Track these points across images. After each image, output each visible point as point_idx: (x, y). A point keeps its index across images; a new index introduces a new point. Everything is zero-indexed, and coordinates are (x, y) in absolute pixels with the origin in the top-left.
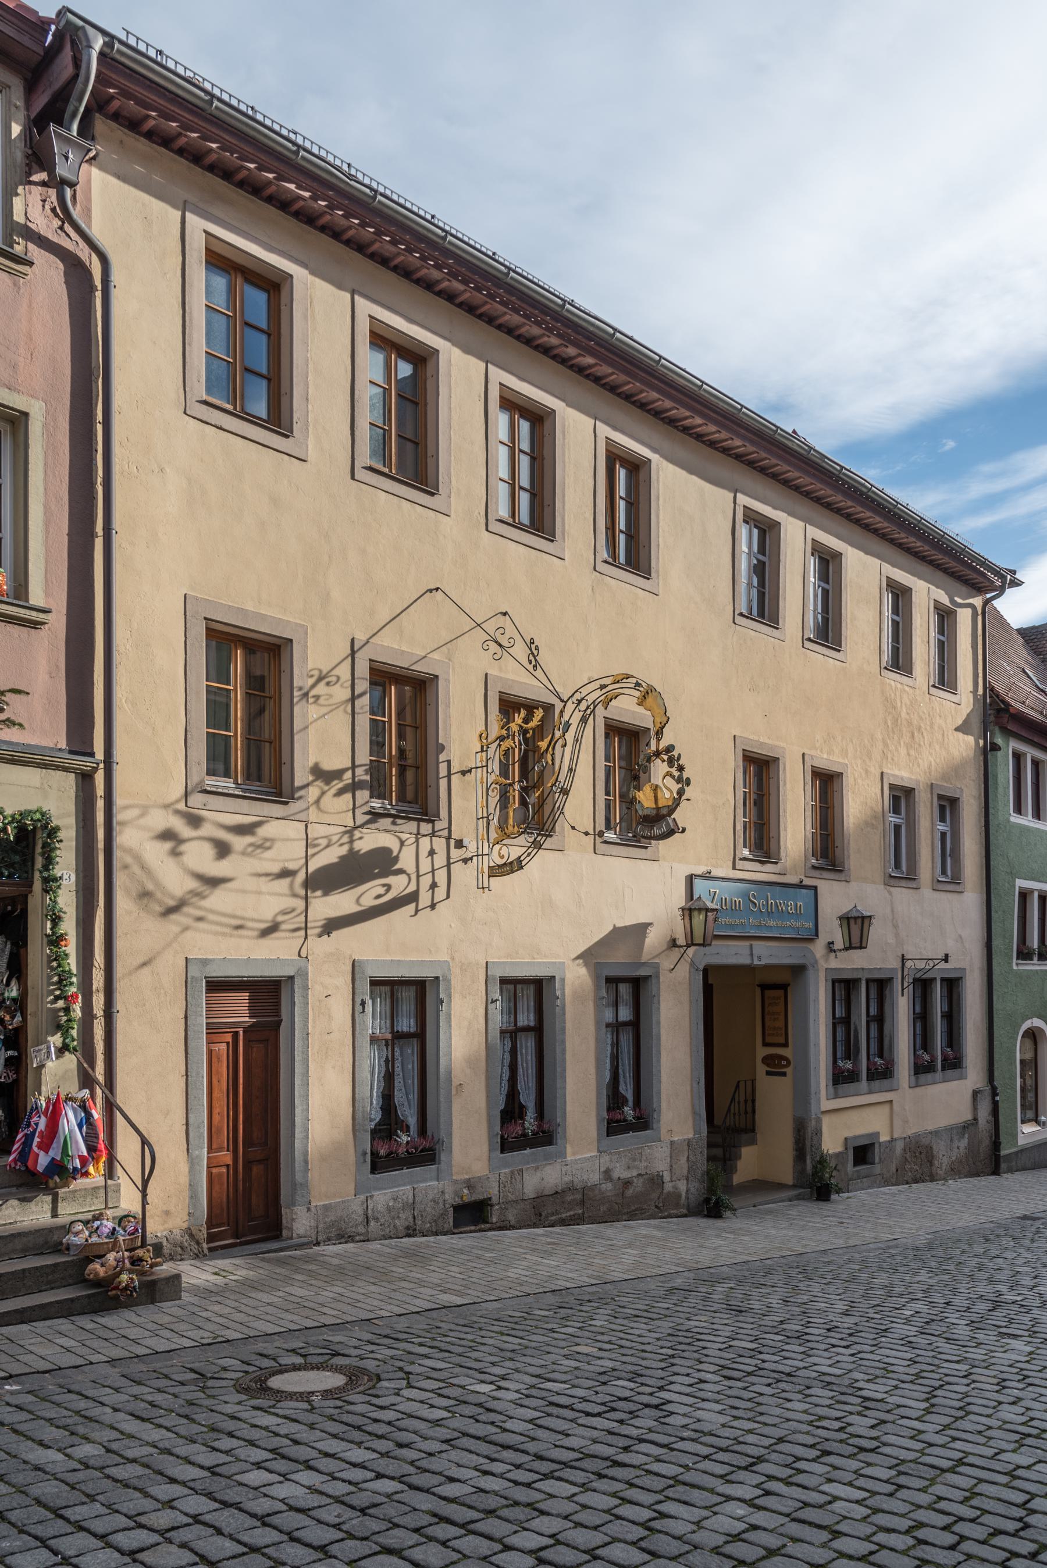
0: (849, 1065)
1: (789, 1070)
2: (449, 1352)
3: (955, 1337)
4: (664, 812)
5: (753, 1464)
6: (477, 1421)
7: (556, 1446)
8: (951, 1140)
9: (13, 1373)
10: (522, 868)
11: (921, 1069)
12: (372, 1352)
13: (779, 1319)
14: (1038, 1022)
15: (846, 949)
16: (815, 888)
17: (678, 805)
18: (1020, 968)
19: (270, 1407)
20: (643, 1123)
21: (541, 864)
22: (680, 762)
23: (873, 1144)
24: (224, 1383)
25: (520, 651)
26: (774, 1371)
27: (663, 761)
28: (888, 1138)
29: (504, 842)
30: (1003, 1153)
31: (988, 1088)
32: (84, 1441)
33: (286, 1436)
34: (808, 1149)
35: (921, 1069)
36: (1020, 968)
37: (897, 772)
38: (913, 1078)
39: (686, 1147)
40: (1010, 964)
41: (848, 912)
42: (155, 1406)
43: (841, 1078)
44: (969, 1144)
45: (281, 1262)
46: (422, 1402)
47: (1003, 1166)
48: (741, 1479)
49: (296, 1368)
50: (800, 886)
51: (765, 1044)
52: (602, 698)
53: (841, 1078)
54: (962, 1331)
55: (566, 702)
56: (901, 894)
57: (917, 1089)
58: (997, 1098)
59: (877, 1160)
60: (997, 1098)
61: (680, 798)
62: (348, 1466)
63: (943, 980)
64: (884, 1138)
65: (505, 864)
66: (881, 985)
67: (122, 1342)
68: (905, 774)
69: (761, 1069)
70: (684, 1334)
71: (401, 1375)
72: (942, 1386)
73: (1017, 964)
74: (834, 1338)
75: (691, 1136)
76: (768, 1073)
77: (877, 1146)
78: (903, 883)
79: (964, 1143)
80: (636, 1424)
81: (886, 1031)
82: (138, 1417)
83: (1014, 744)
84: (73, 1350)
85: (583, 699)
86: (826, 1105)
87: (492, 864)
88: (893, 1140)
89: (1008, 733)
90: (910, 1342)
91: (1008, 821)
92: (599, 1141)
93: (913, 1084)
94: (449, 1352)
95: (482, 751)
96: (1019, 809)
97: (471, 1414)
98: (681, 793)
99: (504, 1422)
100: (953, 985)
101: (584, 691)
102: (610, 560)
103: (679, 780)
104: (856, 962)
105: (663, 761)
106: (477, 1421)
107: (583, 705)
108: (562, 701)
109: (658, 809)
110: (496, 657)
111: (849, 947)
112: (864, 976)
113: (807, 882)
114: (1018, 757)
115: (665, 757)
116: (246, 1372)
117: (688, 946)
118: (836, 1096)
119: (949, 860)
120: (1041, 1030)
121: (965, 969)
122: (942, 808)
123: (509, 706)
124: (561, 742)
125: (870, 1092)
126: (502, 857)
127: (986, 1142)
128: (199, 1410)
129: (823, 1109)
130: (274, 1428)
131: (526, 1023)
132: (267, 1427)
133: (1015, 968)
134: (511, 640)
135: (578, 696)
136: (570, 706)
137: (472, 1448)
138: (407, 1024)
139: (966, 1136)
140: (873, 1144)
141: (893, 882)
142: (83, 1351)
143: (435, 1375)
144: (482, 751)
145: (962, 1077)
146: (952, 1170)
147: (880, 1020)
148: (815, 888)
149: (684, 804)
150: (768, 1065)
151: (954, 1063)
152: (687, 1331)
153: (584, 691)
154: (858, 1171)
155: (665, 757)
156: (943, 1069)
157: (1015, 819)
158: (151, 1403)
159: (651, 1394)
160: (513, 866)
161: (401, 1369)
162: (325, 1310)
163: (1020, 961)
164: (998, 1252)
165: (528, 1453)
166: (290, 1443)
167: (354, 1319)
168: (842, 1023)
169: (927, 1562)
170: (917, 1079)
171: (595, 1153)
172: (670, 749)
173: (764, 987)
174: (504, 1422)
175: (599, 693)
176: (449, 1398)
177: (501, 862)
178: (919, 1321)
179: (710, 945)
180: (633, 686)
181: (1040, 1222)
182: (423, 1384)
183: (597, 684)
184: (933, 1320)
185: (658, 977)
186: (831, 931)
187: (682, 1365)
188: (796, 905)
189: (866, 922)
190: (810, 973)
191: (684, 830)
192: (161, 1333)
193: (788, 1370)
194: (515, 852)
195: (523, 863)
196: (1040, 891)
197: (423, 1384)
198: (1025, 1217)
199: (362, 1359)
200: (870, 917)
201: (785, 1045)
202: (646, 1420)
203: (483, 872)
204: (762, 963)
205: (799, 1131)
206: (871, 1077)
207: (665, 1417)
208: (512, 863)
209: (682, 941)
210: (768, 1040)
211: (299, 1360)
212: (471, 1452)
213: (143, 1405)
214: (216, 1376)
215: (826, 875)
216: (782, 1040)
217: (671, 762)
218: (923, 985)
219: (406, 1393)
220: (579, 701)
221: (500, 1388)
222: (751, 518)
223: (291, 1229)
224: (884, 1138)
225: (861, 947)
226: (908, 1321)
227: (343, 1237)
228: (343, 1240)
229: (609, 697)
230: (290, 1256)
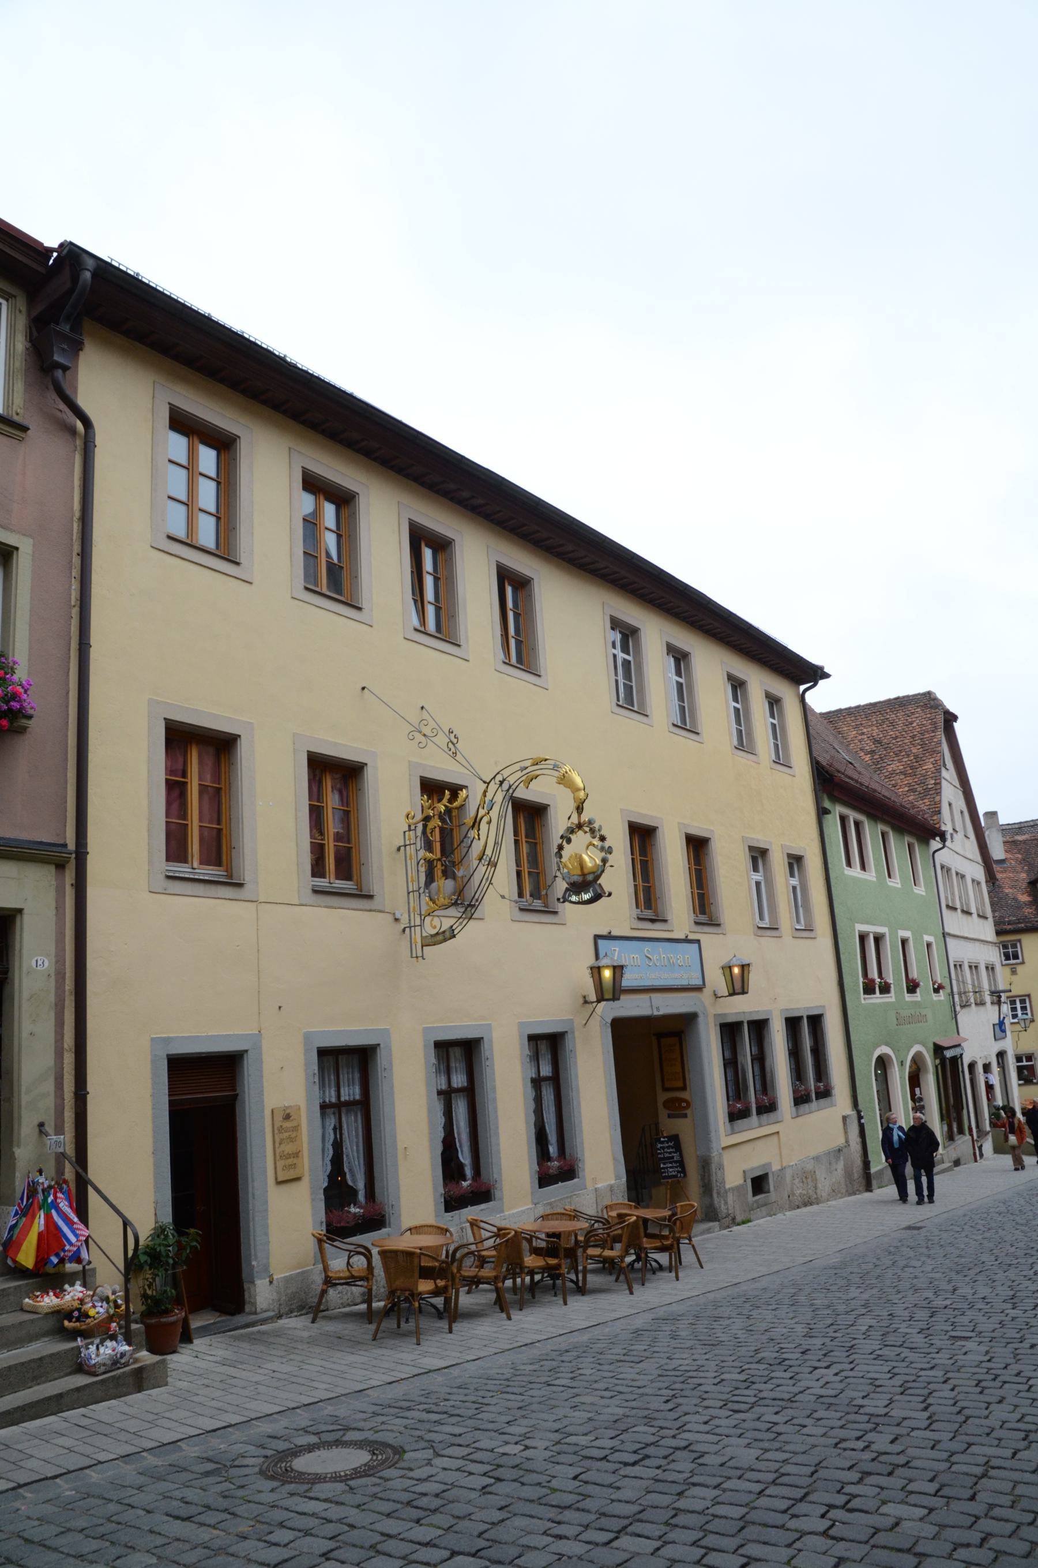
0: (289, 1148)
1: (688, 1112)
2: (459, 1415)
3: (914, 1345)
4: (590, 878)
5: (806, 1494)
6: (523, 1484)
7: (613, 1501)
8: (830, 1164)
9: (22, 1482)
10: (454, 936)
11: (800, 1099)
12: (383, 1423)
13: (753, 1348)
14: (885, 1050)
15: (730, 995)
16: (698, 941)
17: (603, 871)
18: (868, 1001)
19: (307, 1491)
20: (569, 1173)
21: (471, 933)
22: (602, 833)
23: (766, 1175)
24: (246, 1471)
25: (442, 740)
26: (774, 1399)
27: (586, 832)
28: (779, 1167)
29: (435, 913)
30: (873, 1170)
31: (854, 1113)
32: (130, 1551)
33: (340, 1521)
34: (714, 1185)
35: (800, 1099)
36: (868, 1001)
37: (753, 836)
38: (794, 1109)
39: (609, 1193)
40: (859, 998)
41: (730, 961)
42: (187, 1503)
43: (736, 1115)
44: (844, 1166)
45: (251, 1339)
46: (458, 1470)
47: (874, 1183)
48: (803, 1512)
49: (311, 1448)
50: (687, 940)
51: (665, 1089)
52: (524, 778)
53: (736, 1115)
54: (919, 1340)
55: (489, 783)
56: (767, 942)
57: (799, 1119)
58: (863, 1121)
59: (772, 1188)
60: (863, 1121)
61: (604, 865)
62: (418, 1547)
63: (750, 1023)
64: (776, 1167)
65: (437, 934)
66: (759, 1027)
67: (123, 1436)
68: (760, 837)
69: (663, 1113)
70: (673, 1373)
71: (424, 1444)
72: (930, 1393)
73: (864, 999)
74: (812, 1358)
75: (613, 1182)
76: (669, 1116)
77: (770, 1176)
78: (769, 933)
79: (840, 1166)
80: (678, 1469)
81: (768, 1069)
82: (177, 1518)
83: (838, 809)
84: (75, 1449)
85: (504, 780)
86: (726, 1141)
87: (424, 934)
88: (783, 1169)
89: (834, 799)
90: (879, 1356)
91: (843, 873)
92: (532, 1193)
93: (794, 1115)
94: (459, 1415)
95: (410, 830)
96: (849, 864)
97: (514, 1477)
98: (604, 861)
99: (549, 1482)
100: (816, 1021)
101: (506, 773)
102: (507, 661)
103: (602, 849)
104: (741, 1008)
105: (586, 832)
106: (523, 1484)
107: (505, 786)
108: (485, 782)
109: (584, 875)
110: (421, 745)
111: (733, 993)
112: (745, 1019)
113: (691, 937)
114: (843, 819)
115: (587, 829)
116: (267, 1457)
117: (599, 1001)
118: (733, 1132)
119: (801, 910)
120: (889, 1057)
121: (824, 1006)
122: (791, 865)
123: (431, 788)
124: (485, 819)
125: (760, 1126)
126: (435, 927)
127: (858, 1162)
128: (238, 1502)
129: (723, 1145)
130: (323, 1514)
131: (347, 1098)
132: (226, 1510)
133: (863, 1002)
134: (412, 738)
135: (499, 778)
136: (493, 787)
137: (533, 1513)
138: (351, 1092)
139: (842, 1158)
140: (766, 1175)
141: (760, 932)
142: (88, 1450)
143: (458, 1441)
144: (410, 830)
145: (833, 1105)
146: (834, 1191)
147: (761, 1058)
148: (698, 941)
149: (608, 869)
150: (669, 1108)
151: (825, 1093)
152: (674, 1370)
153: (506, 773)
154: (756, 1201)
155: (587, 829)
156: (817, 1099)
157: (848, 871)
158: (182, 1500)
159: (674, 1437)
160: (450, 934)
161: (421, 1438)
162: (315, 1384)
163: (866, 996)
164: (905, 1262)
165: (588, 1511)
166: (347, 1528)
167: (348, 1391)
168: (731, 1064)
169: (674, 1561)
170: (797, 1110)
171: (530, 1206)
172: (590, 822)
173: (660, 1036)
174: (549, 1482)
175: (519, 774)
176: (483, 1463)
177: (434, 932)
178: (876, 1334)
179: (618, 999)
180: (551, 767)
181: (924, 1229)
182: (450, 1451)
183: (517, 767)
184: (888, 1332)
185: (573, 1032)
186: (716, 981)
187: (688, 1404)
188: (684, 957)
189: (746, 968)
190: (701, 1020)
191: (610, 895)
192: (159, 1422)
193: (786, 1396)
194: (447, 923)
195: (455, 932)
196: (875, 933)
197: (450, 1451)
198: (909, 1228)
199: (377, 1432)
200: (749, 965)
201: (684, 1088)
202: (684, 1463)
203: (416, 942)
204: (661, 1013)
205: (704, 1167)
206: (759, 1112)
207: (699, 1458)
208: (444, 932)
209: (593, 997)
210: (668, 1085)
211: (314, 1439)
212: (532, 1517)
213: (175, 1503)
214: (236, 1463)
215: (706, 929)
216: (680, 1084)
217: (592, 831)
218: (793, 1023)
219: (438, 1462)
220: (501, 783)
221: (527, 1447)
222: (616, 624)
223: (254, 1304)
224: (776, 1167)
225: (744, 992)
226: (866, 1335)
227: (303, 1308)
228: (304, 1312)
229: (530, 778)
230: (259, 1332)
